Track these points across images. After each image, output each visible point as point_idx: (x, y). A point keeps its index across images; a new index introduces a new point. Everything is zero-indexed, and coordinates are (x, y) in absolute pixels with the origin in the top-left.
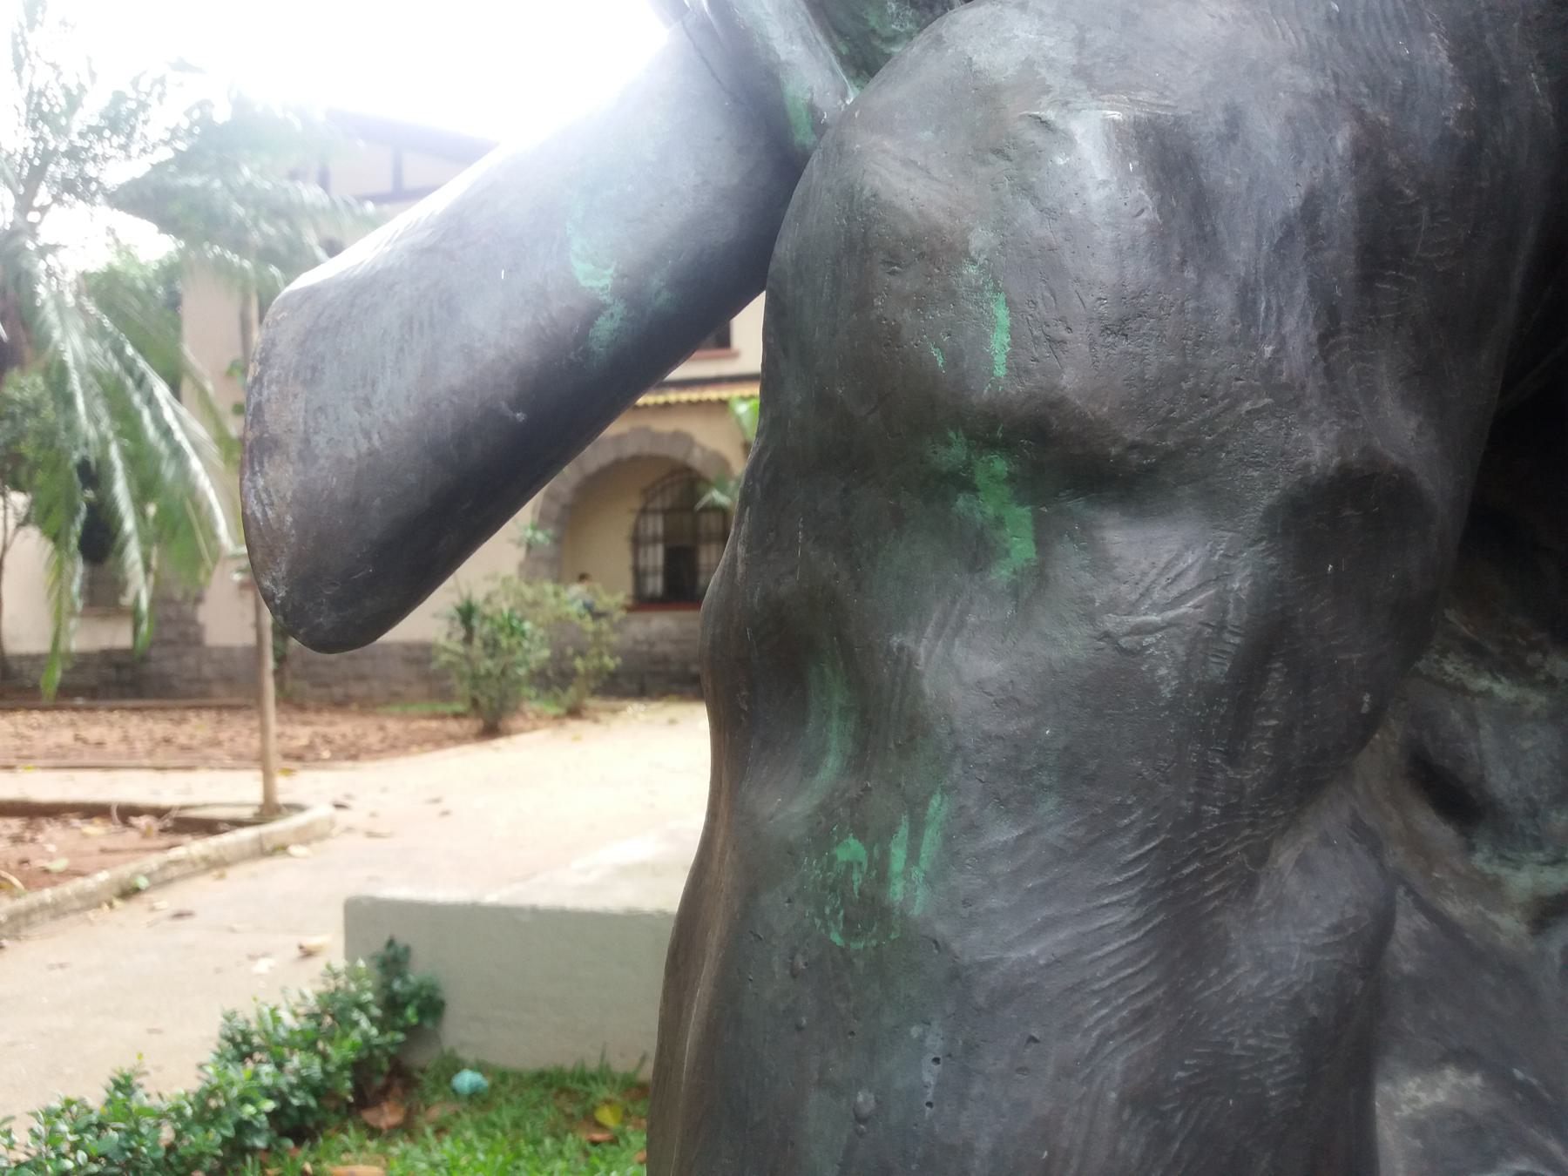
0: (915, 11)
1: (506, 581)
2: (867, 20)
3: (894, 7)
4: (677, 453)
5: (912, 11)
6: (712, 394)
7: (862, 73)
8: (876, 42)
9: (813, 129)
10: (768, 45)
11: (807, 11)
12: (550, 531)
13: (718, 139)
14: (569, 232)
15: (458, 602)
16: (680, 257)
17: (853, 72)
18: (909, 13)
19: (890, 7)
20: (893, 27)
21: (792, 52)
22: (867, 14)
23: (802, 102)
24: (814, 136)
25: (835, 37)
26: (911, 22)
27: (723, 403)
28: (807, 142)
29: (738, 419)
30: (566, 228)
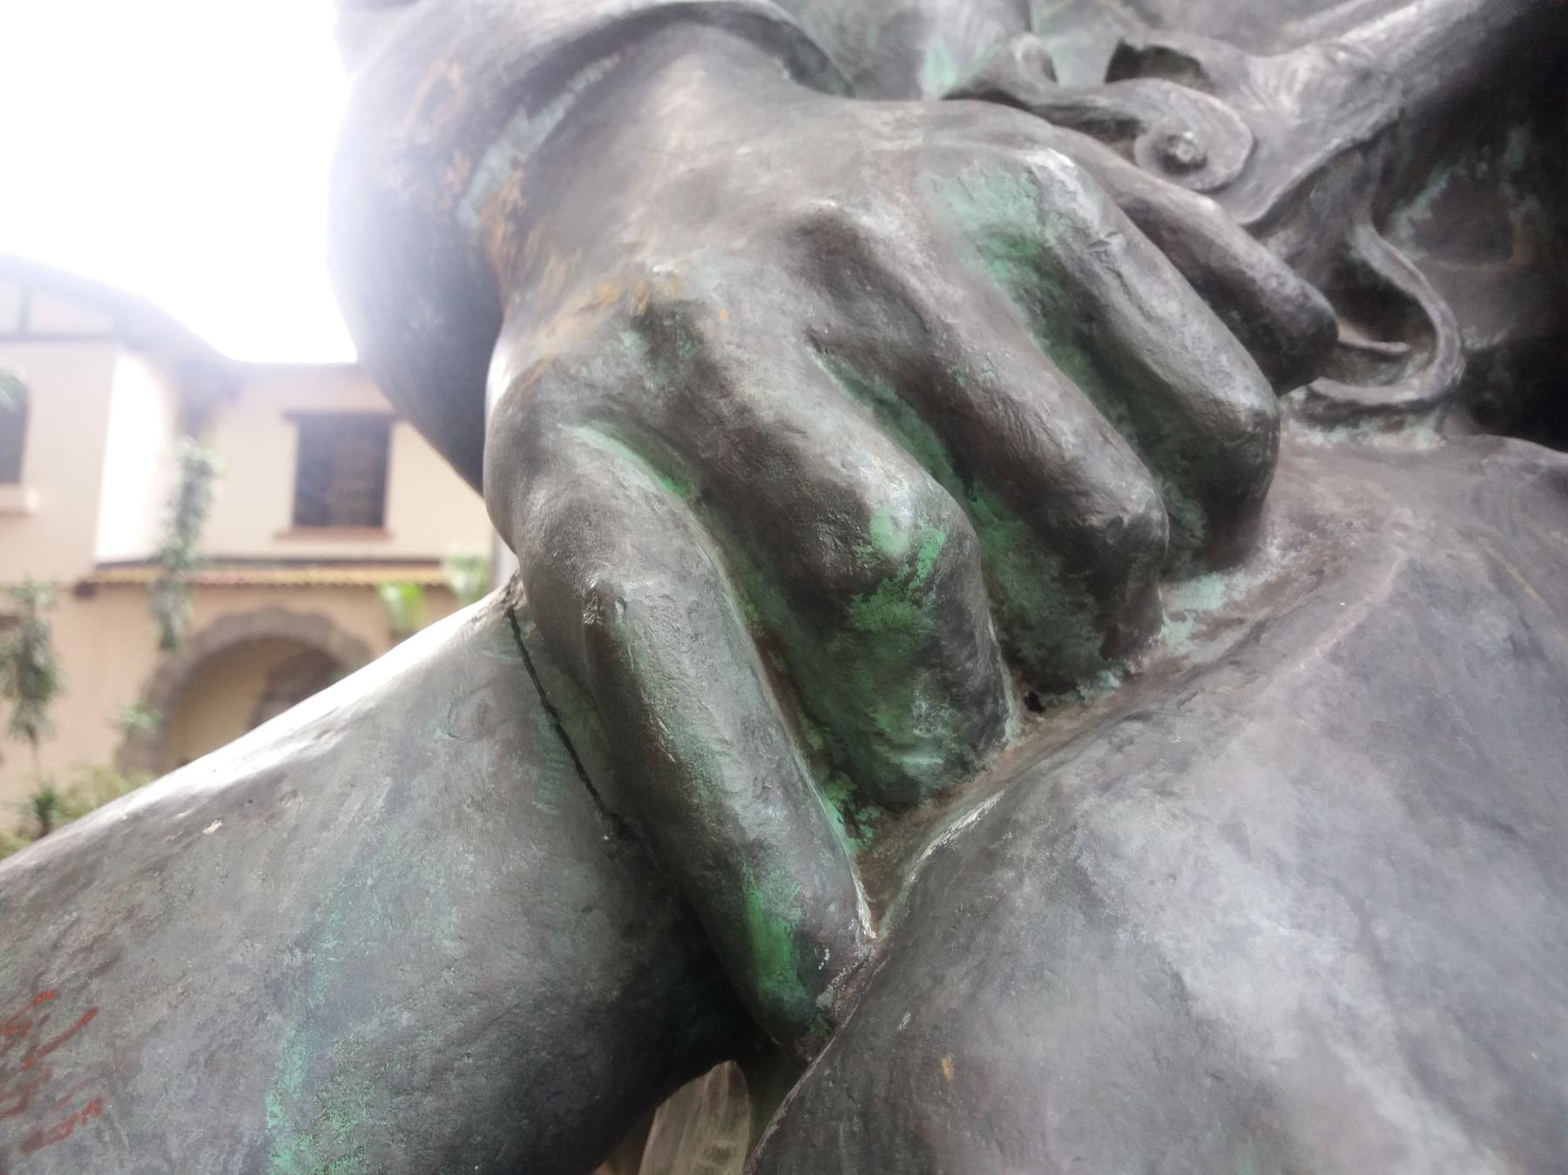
0: (955, 711)
1: (97, 774)
2: (874, 719)
3: (924, 706)
4: (313, 635)
5: (951, 710)
6: (359, 576)
7: (839, 777)
8: (881, 749)
9: (799, 976)
10: (721, 805)
11: (781, 718)
12: (158, 714)
13: (588, 909)
14: (271, 1123)
15: (35, 789)
16: (495, 1155)
17: (824, 772)
18: (945, 714)
19: (920, 707)
20: (916, 732)
21: (768, 821)
22: (875, 711)
23: (783, 924)
24: (801, 988)
25: (805, 722)
26: (945, 725)
27: (370, 590)
28: (786, 998)
29: (385, 605)
30: (264, 1111)
